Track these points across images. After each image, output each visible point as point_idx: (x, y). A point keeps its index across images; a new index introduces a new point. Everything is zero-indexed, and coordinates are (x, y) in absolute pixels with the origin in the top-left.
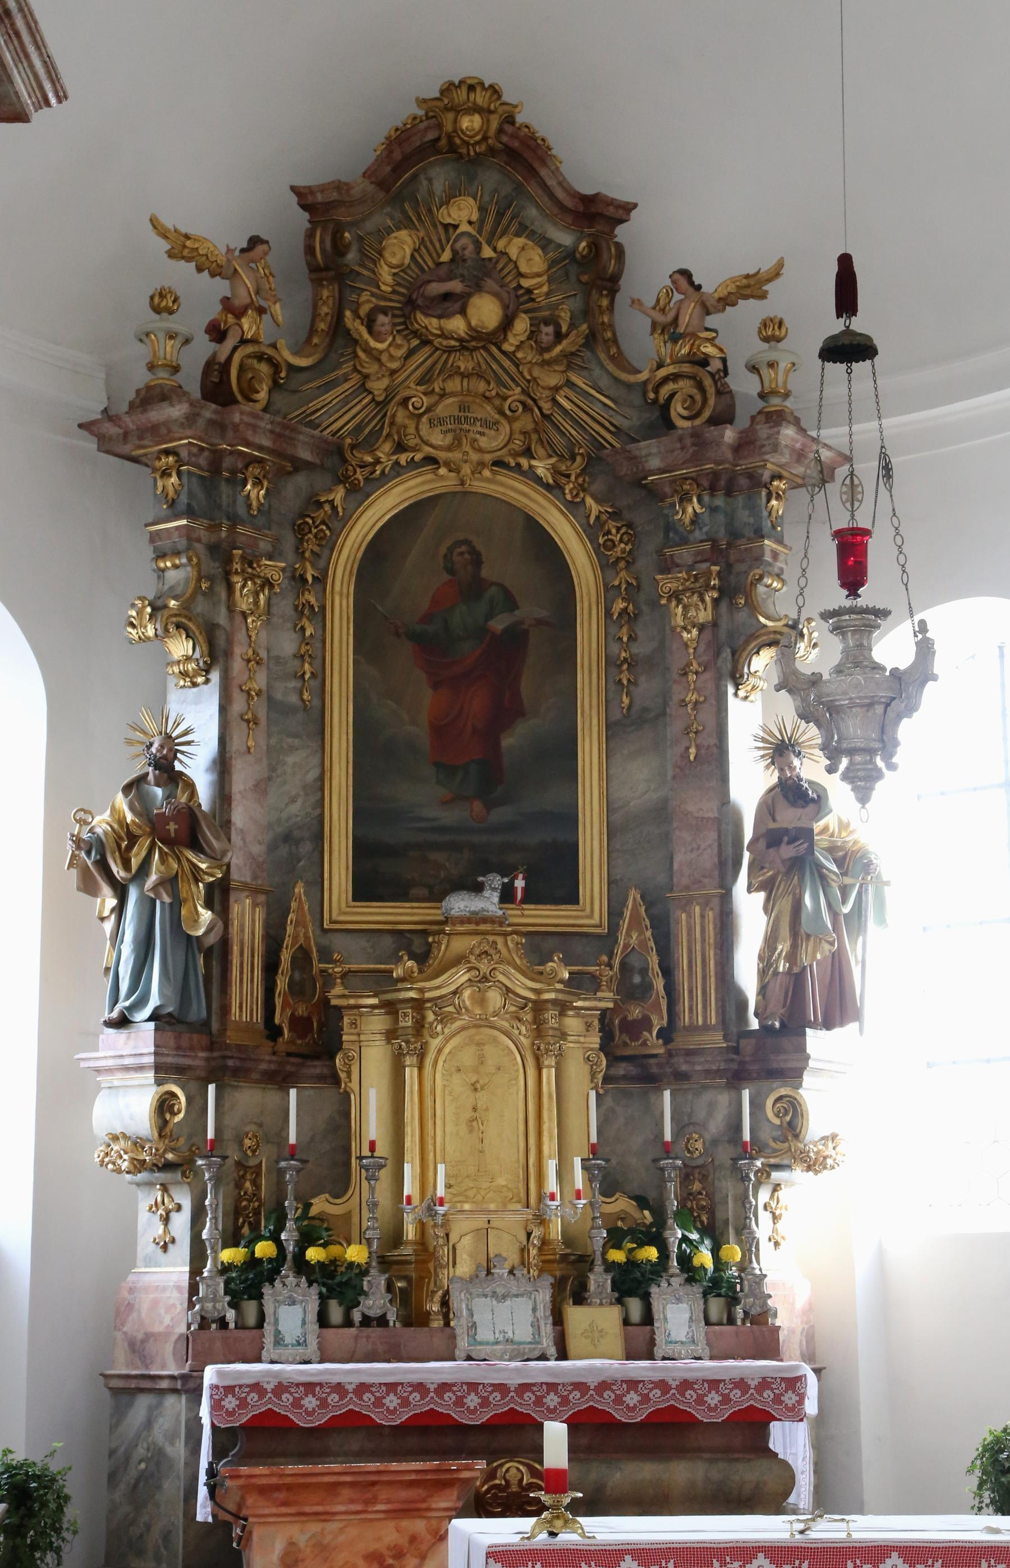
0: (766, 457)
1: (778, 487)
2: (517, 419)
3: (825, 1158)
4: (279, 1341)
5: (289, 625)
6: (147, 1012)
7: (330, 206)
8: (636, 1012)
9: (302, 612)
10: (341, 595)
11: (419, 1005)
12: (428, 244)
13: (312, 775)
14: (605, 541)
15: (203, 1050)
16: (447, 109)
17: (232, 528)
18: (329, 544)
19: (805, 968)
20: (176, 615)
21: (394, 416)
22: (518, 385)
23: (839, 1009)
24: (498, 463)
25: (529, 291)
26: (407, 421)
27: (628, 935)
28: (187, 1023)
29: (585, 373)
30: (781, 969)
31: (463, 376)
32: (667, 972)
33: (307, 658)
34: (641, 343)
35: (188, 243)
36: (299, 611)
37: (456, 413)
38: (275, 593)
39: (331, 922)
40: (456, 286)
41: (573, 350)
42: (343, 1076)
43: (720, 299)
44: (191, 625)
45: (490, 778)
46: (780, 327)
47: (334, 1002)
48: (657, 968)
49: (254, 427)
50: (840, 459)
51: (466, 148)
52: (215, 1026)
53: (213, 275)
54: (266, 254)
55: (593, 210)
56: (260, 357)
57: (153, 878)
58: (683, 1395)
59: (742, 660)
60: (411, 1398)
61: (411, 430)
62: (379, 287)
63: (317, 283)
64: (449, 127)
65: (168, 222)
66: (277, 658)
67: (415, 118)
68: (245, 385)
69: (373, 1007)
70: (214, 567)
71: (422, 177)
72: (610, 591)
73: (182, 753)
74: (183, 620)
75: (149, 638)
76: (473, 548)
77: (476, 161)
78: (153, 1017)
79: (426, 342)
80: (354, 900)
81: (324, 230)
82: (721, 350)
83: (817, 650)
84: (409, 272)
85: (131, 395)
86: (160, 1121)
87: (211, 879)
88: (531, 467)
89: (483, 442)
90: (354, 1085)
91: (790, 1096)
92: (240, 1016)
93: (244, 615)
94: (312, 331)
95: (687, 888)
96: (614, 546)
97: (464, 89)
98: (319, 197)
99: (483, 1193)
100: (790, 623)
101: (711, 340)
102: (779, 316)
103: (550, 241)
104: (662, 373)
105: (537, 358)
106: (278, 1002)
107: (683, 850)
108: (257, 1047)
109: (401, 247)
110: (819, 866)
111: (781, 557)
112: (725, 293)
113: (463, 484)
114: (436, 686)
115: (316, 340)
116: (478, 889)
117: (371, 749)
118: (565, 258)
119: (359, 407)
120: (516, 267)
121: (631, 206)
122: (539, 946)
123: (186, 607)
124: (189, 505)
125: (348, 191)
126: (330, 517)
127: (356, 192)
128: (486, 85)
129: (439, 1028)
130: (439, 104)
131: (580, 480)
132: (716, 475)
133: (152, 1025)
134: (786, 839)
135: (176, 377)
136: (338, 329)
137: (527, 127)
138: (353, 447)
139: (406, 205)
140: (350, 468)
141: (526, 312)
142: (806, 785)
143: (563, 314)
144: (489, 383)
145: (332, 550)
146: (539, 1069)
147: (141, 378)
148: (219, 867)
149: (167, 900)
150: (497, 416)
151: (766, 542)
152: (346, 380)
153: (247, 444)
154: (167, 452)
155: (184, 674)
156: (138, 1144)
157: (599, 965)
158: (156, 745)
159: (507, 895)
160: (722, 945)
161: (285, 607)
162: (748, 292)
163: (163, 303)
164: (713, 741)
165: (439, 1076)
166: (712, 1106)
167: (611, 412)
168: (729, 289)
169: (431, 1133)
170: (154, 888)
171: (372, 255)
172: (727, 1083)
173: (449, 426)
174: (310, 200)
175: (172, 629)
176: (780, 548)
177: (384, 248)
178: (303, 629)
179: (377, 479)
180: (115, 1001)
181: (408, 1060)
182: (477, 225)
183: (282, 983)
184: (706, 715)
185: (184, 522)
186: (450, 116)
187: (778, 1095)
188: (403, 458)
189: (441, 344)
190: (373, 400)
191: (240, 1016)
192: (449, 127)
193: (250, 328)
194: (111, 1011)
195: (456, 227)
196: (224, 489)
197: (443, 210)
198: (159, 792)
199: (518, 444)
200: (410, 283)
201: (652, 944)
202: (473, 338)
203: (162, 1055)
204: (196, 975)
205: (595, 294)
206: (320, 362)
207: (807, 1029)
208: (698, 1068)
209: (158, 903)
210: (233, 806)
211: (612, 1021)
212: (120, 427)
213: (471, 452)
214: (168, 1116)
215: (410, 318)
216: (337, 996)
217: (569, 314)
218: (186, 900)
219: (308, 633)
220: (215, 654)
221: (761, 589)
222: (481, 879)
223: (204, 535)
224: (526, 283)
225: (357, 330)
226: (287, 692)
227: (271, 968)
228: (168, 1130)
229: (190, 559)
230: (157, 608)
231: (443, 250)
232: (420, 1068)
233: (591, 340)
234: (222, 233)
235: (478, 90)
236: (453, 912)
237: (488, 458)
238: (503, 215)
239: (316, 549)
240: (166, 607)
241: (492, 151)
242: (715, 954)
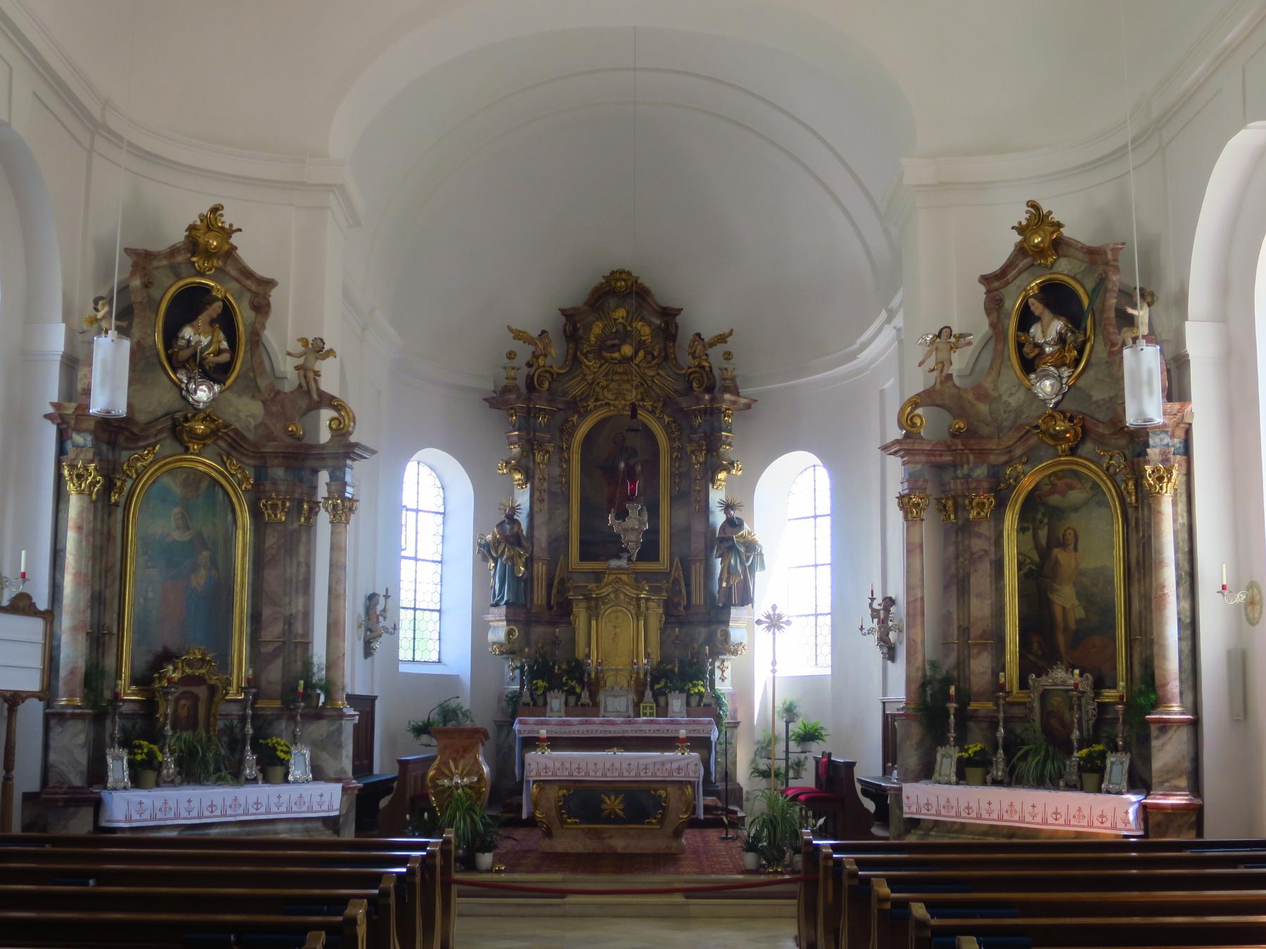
4: (552, 710)
8: (676, 600)
11: (597, 599)
18: (571, 435)
34: (687, 361)
36: (561, 460)
40: (616, 342)
63: (568, 342)
72: (672, 449)
78: (506, 603)
109: (597, 329)
122: (639, 577)
123: (518, 462)
132: (706, 409)
147: (505, 382)
156: (501, 645)
171: (588, 329)
183: (554, 591)
216: (571, 595)
220: (529, 477)
230: (508, 463)
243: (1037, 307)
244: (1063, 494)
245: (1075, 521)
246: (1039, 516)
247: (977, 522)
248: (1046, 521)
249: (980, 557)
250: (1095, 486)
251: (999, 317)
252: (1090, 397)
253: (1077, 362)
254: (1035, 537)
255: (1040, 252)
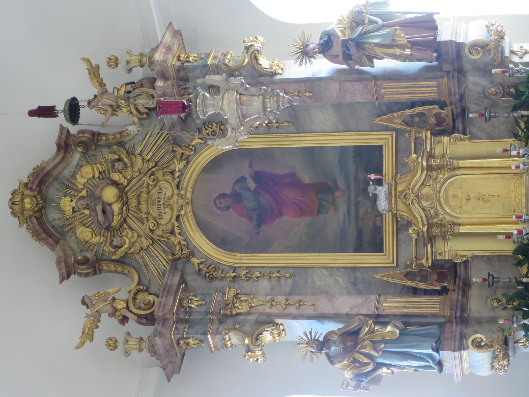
0: (169, 65)
1: (184, 57)
2: (157, 178)
3: (497, 31)
5: (255, 284)
6: (435, 354)
7: (67, 266)
8: (433, 120)
9: (250, 277)
10: (240, 259)
11: (430, 226)
12: (82, 219)
13: (325, 272)
14: (212, 135)
15: (452, 327)
16: (23, 213)
17: (212, 313)
18: (217, 266)
19: (408, 41)
20: (252, 341)
21: (158, 236)
22: (142, 177)
23: (428, 23)
24: (178, 187)
25: (100, 173)
26: (161, 229)
27: (396, 123)
28: (440, 335)
29: (136, 146)
30: (409, 53)
31: (139, 204)
32: (413, 105)
33: (271, 275)
35: (86, 332)
36: (249, 279)
37: (156, 207)
38: (241, 292)
39: (393, 263)
40: (99, 208)
41: (125, 152)
42: (464, 259)
43: (100, 86)
44: (256, 333)
45: (324, 189)
46: (111, 59)
47: (430, 264)
48: (411, 110)
49: (165, 305)
50: (170, 29)
51: (38, 204)
52: (442, 320)
53: (99, 321)
54: (89, 297)
55: (63, 145)
56: (134, 299)
57: (373, 352)
59: (264, 72)
61: (164, 227)
62: (102, 243)
63: (101, 271)
64: (30, 213)
65: (78, 341)
66: (272, 289)
67: (27, 228)
68: (147, 307)
69: (432, 246)
70: (229, 322)
71: (53, 223)
73: (315, 336)
74: (254, 337)
75: (263, 353)
76: (217, 197)
77: (45, 199)
78: (437, 351)
79: (125, 221)
80: (383, 252)
81: (78, 269)
82: (122, 86)
83: (258, 37)
84: (94, 229)
85: (154, 359)
86: (485, 347)
87: (373, 325)
88: (179, 171)
89: (169, 194)
90: (469, 254)
91: (469, 48)
92: (437, 308)
93: (251, 307)
94: (122, 273)
95: (373, 95)
96: (214, 131)
97: (14, 206)
98: (64, 271)
99: (517, 195)
100: (246, 51)
101: (118, 90)
102: (106, 60)
103: (78, 164)
104: (134, 111)
105: (130, 169)
106: (430, 287)
107: (355, 97)
108: (451, 300)
109: (84, 233)
110: (360, 35)
111: (216, 54)
112: (97, 83)
113: (187, 203)
114: (281, 214)
115: (126, 272)
116: (375, 196)
117: (313, 244)
118: (85, 156)
119: (155, 252)
120: (90, 179)
121: (61, 127)
122: (400, 167)
124: (202, 334)
125: (60, 258)
126: (206, 265)
127: (61, 254)
128: (12, 197)
129: (441, 216)
130: (21, 217)
131: (184, 148)
133: (441, 352)
134: (347, 52)
135: (145, 339)
136: (120, 262)
137: (29, 177)
138: (173, 254)
139: (66, 230)
140: (183, 256)
141: (110, 174)
142: (322, 41)
143: (110, 157)
144: (142, 192)
145: (221, 264)
146: (459, 168)
147: (145, 353)
148: (367, 321)
149: (383, 346)
150: (157, 188)
151: (209, 63)
152: (143, 257)
153: (173, 307)
154: (178, 344)
155: (279, 335)
157: (410, 137)
158: (312, 350)
159: (379, 182)
160: (400, 79)
161: (247, 286)
162: (96, 73)
163: (112, 344)
164: (303, 85)
165: (463, 217)
166: (475, 84)
167: (153, 133)
168: (96, 82)
169: (490, 219)
170: (377, 352)
171: (86, 245)
172: (464, 77)
173: (162, 210)
174: (65, 275)
175: (259, 342)
176: (212, 56)
177: (84, 240)
178: (257, 277)
179: (187, 243)
180: (429, 367)
181: (456, 231)
182: (72, 197)
183: (422, 286)
184: (291, 88)
185: (209, 337)
186: (26, 213)
187: (469, 53)
188: (177, 231)
189: (125, 214)
190: (152, 245)
191: (437, 308)
192: (30, 213)
193: (121, 304)
194: (434, 369)
195: (73, 208)
196: (193, 317)
197: (67, 213)
198: (333, 348)
199: (169, 177)
200: (99, 228)
201: (400, 113)
202: (122, 199)
203: (454, 348)
204: (417, 331)
205: (101, 143)
206: (135, 269)
207: (437, 40)
208: (457, 91)
209: (384, 350)
210: (339, 313)
211: (437, 130)
212: (168, 365)
213: (174, 200)
214: (483, 344)
215: (114, 229)
217: (110, 154)
218: (383, 337)
219: (259, 275)
220: (269, 321)
221: (231, 64)
222: (371, 195)
223: (216, 326)
224: (97, 175)
225: (121, 253)
226: (287, 285)
227: (415, 291)
228: (489, 344)
229: (226, 334)
231: (84, 213)
232: (460, 225)
233: (121, 144)
234: (80, 316)
235: (14, 200)
236: (387, 208)
237: (176, 191)
238: (67, 186)
239: (220, 271)
240: (248, 345)
241: (40, 192)
242: (404, 82)
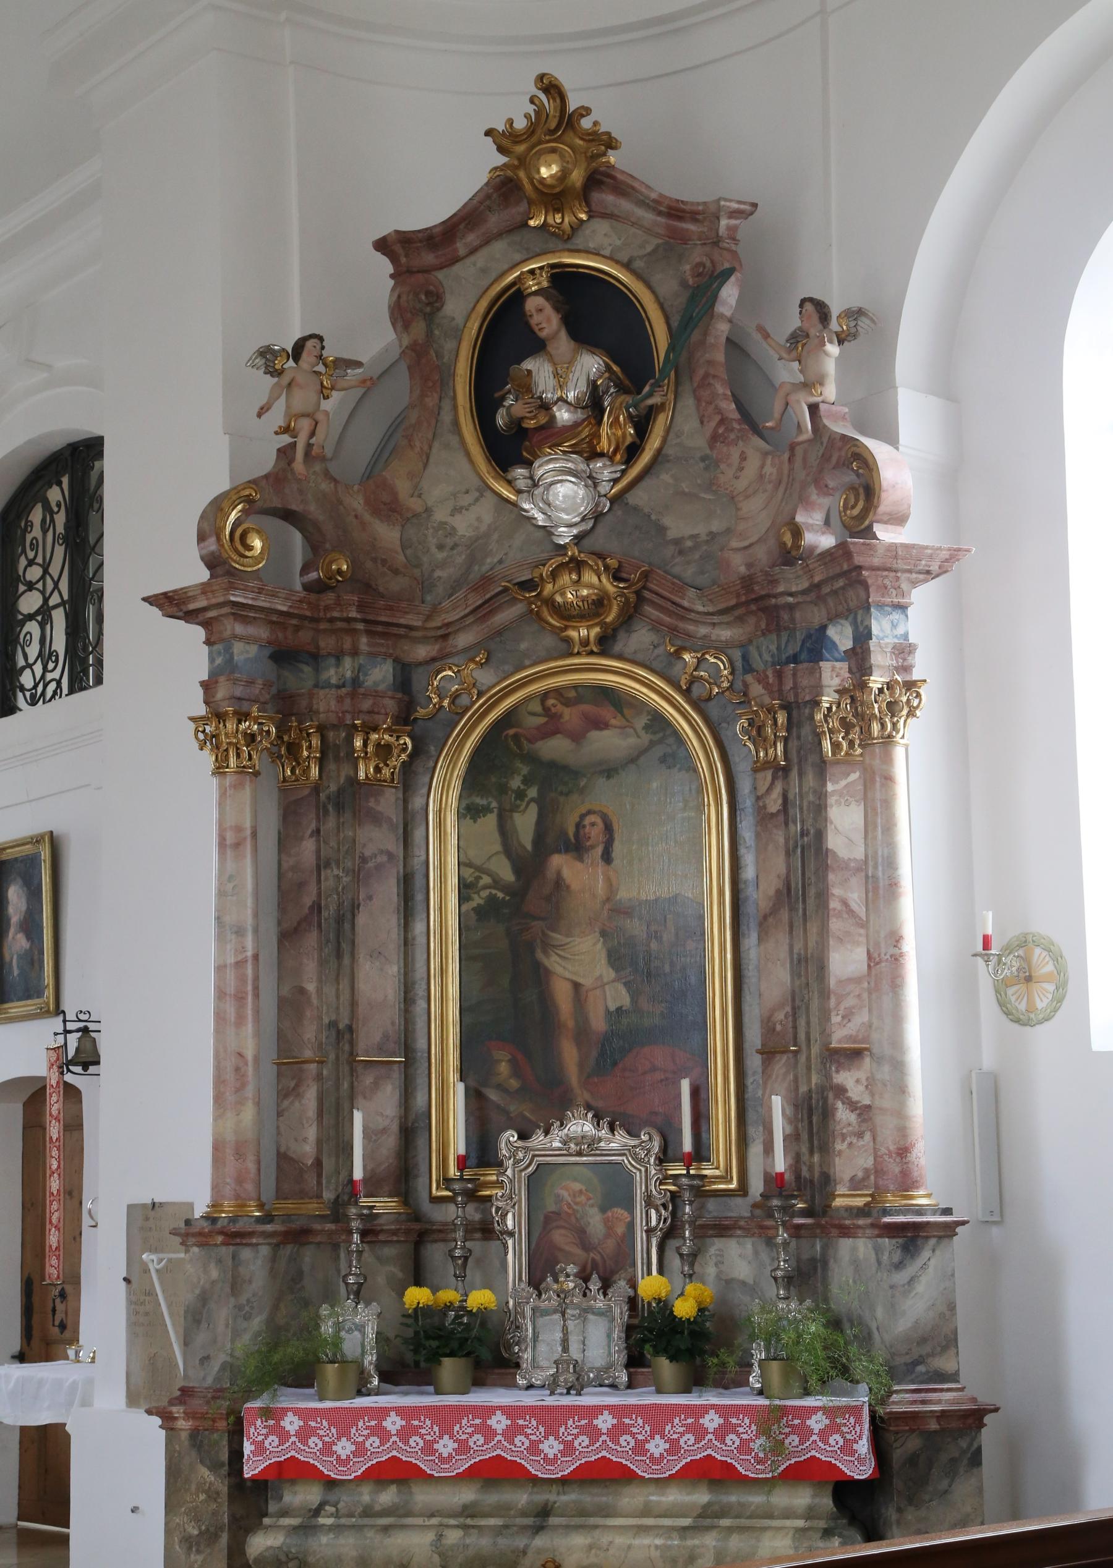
39: (717, 1168)
58: (406, 1443)
60: (576, 1443)
243: (544, 317)
244: (577, 737)
245: (603, 796)
246: (516, 783)
247: (373, 786)
248: (533, 792)
249: (379, 867)
250: (658, 721)
251: (429, 334)
252: (662, 530)
253: (633, 452)
254: (505, 830)
255: (554, 197)
